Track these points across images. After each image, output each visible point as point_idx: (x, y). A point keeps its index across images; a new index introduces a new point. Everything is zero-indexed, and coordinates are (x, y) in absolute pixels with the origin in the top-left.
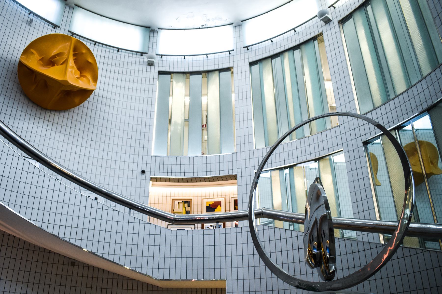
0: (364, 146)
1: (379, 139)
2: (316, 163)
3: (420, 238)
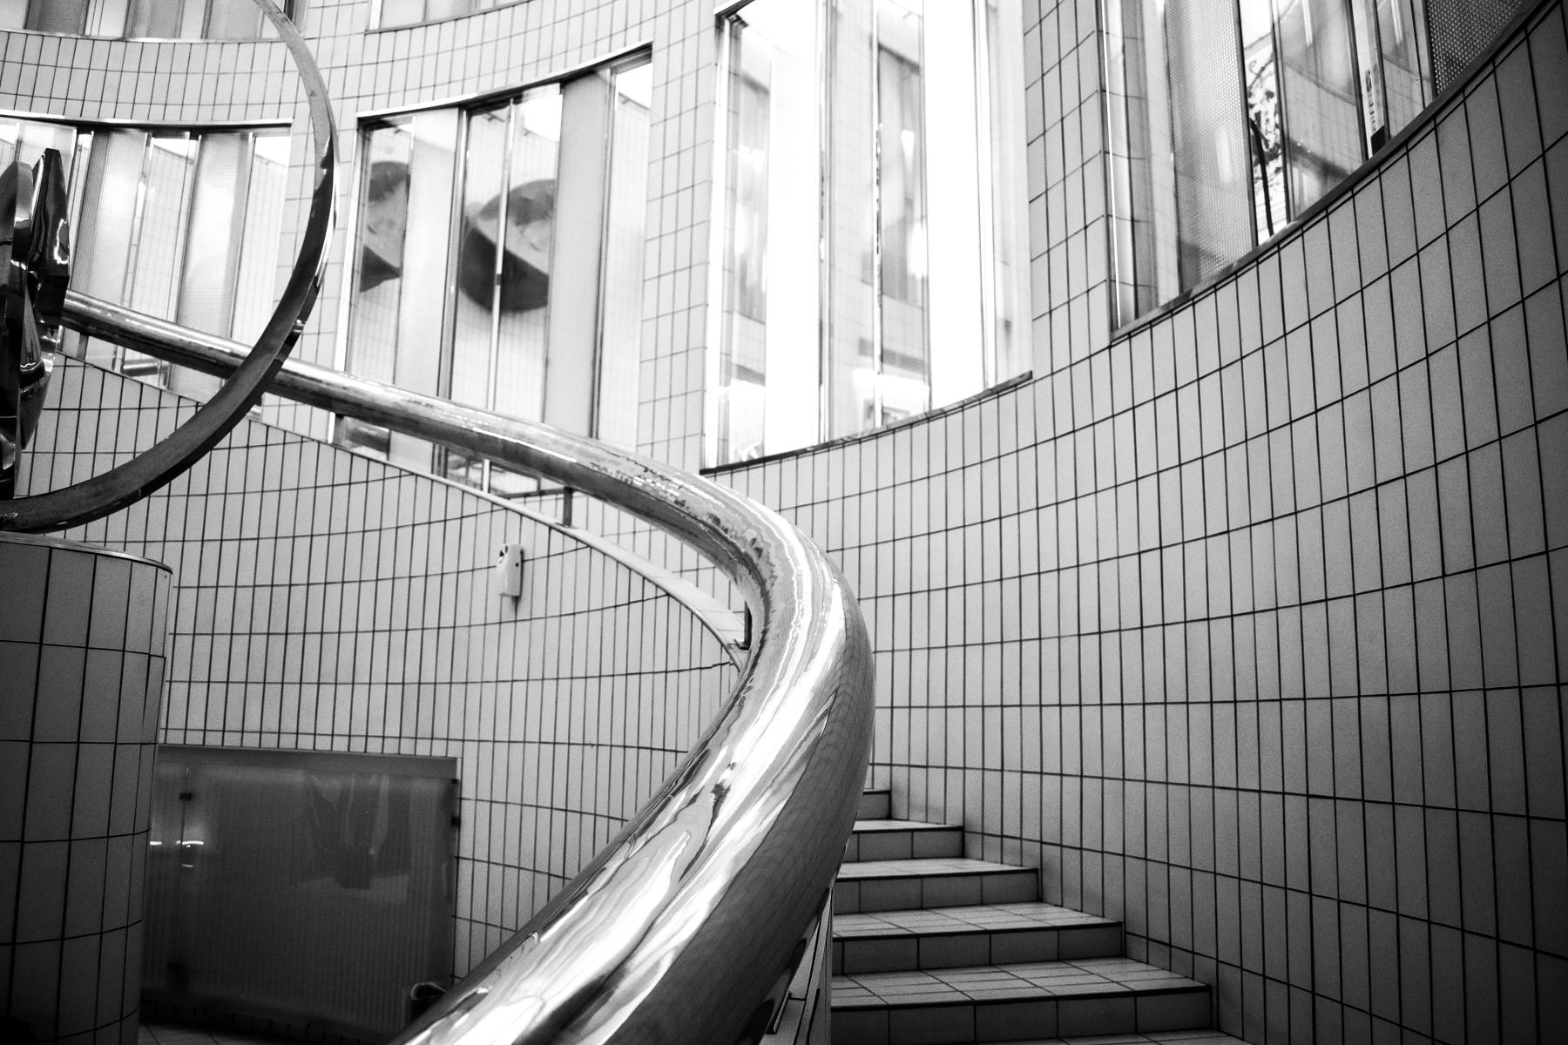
0: (361, 131)
1: (517, 190)
2: (194, 142)
3: (437, 446)
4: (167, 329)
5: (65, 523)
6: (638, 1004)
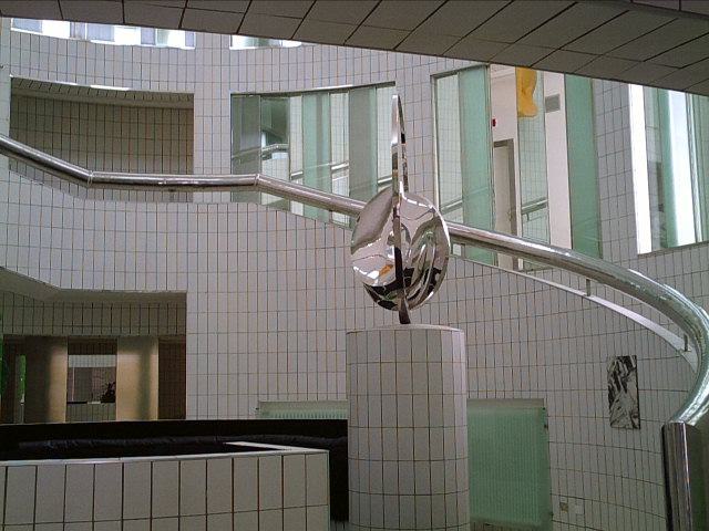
4: (660, 175)
5: (23, 445)
6: (638, 219)
